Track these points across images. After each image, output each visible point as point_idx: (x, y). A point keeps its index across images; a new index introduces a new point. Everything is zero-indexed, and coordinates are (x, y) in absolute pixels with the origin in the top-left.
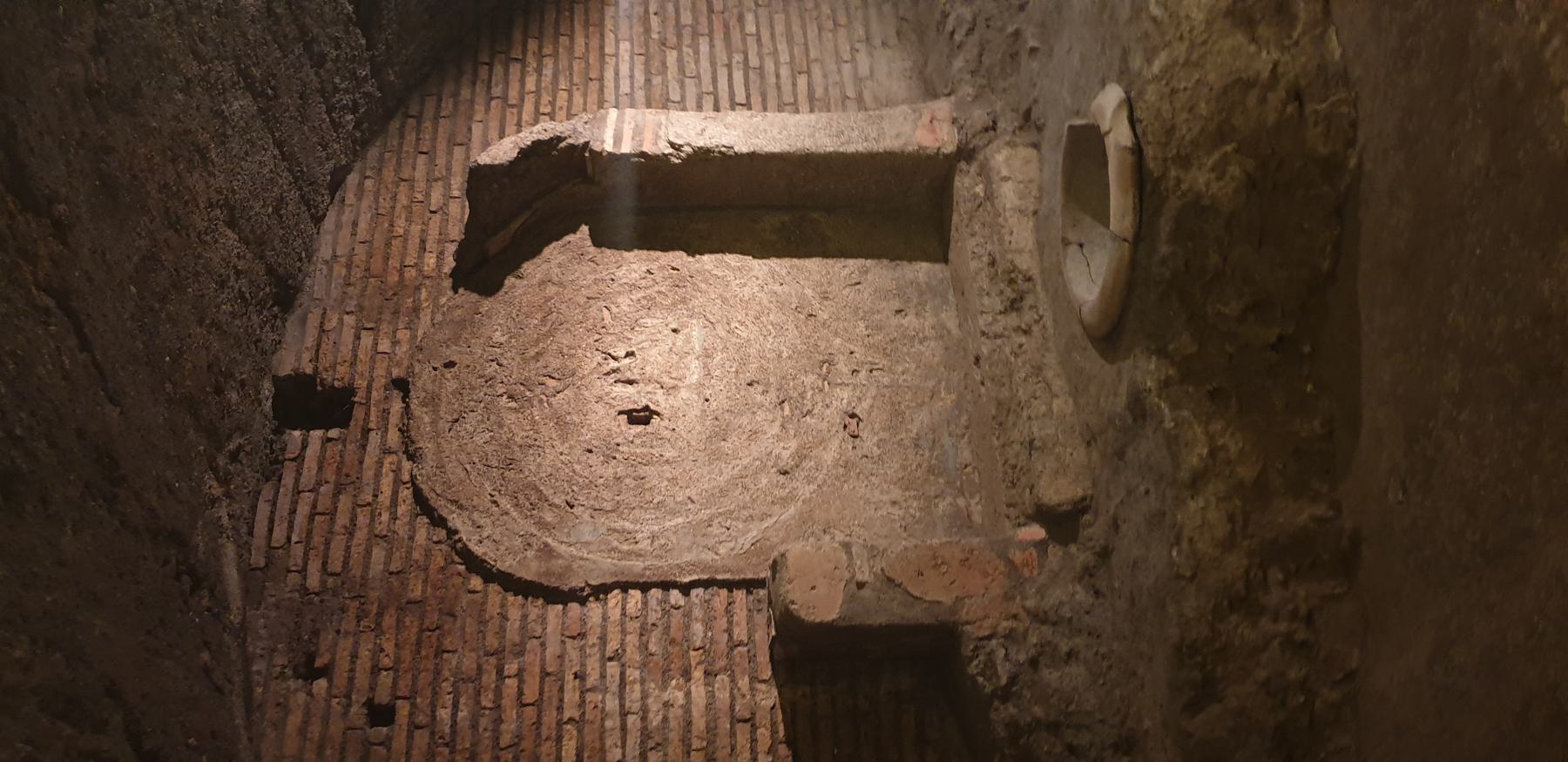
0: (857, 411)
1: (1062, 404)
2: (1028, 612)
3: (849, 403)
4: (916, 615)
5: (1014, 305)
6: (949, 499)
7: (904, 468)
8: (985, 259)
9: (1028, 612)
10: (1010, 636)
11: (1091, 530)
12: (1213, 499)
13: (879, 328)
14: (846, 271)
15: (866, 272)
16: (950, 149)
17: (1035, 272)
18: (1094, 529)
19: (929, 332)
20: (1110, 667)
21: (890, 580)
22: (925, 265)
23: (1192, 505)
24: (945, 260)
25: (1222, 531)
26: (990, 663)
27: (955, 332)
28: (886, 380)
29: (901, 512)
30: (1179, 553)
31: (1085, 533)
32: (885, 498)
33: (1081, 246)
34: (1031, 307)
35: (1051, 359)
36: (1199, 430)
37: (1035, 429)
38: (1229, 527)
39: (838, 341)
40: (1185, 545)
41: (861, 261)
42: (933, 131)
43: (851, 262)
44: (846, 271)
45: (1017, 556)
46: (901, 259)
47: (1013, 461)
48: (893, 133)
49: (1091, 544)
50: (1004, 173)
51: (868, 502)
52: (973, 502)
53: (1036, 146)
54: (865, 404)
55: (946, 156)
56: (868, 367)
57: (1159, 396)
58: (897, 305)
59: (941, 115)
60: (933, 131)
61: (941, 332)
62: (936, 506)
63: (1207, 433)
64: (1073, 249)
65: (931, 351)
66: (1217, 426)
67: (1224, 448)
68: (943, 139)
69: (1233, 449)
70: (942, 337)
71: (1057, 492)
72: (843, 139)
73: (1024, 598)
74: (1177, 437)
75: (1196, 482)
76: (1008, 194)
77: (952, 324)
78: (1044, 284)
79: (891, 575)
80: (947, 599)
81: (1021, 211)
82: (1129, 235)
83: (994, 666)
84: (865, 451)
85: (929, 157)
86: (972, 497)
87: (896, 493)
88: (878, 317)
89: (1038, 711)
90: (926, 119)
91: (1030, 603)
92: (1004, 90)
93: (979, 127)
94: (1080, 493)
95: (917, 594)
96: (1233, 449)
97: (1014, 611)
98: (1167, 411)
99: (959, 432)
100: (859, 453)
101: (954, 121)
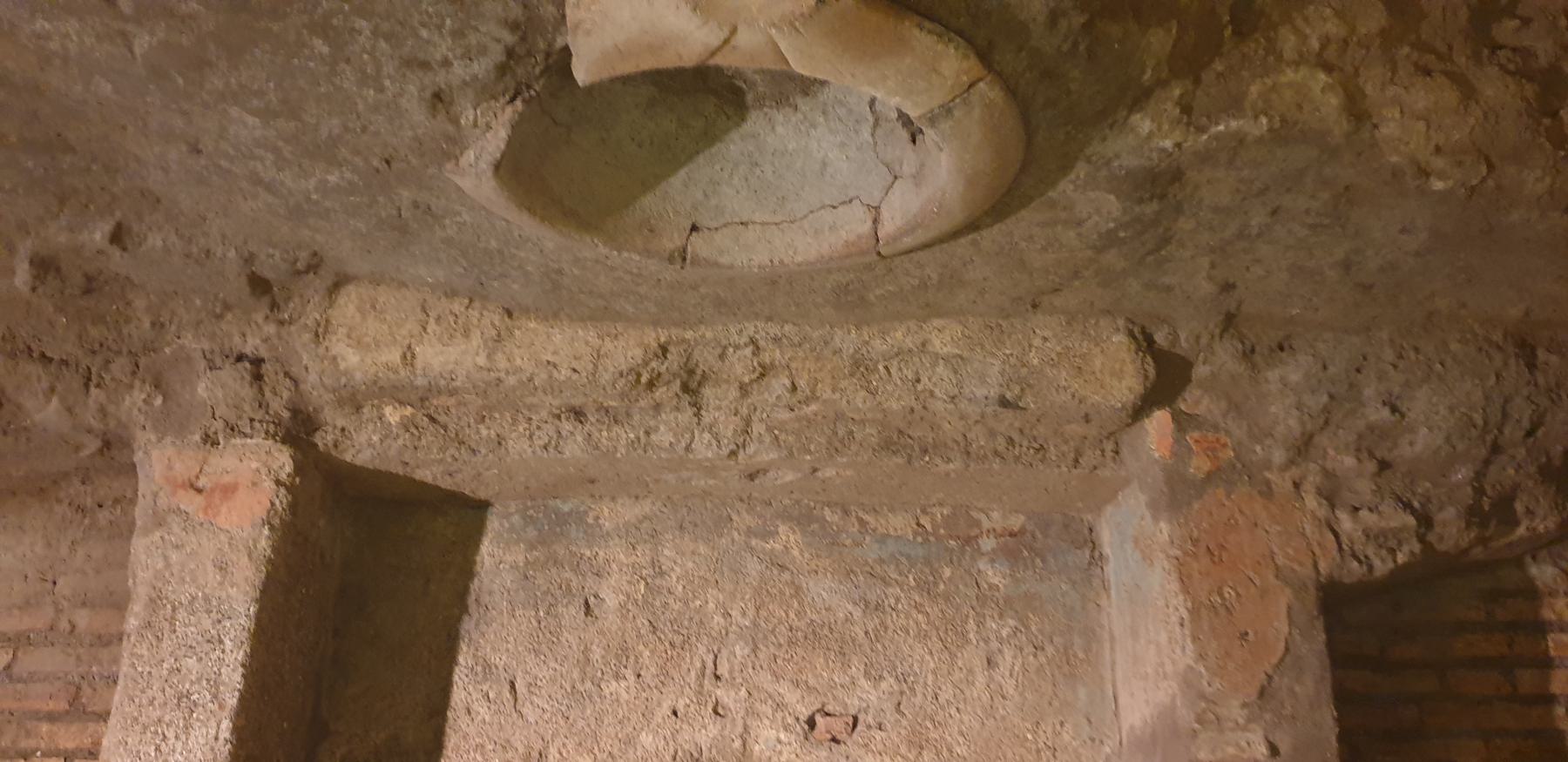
0: (804, 713)
1: (943, 338)
2: (1291, 462)
3: (786, 728)
4: (1313, 648)
5: (691, 386)
6: (982, 565)
7: (923, 636)
8: (567, 426)
9: (1291, 462)
10: (1330, 497)
11: (1183, 337)
12: (1391, 91)
13: (624, 651)
14: (482, 710)
15: (488, 667)
16: (283, 460)
17: (652, 337)
18: (1181, 335)
19: (643, 555)
20: (1417, 350)
21: (1262, 693)
22: (486, 547)
23: (1389, 130)
24: (483, 506)
25: (1451, 96)
26: (1376, 537)
27: (646, 507)
28: (741, 650)
29: (1008, 653)
30: (1442, 176)
31: (1184, 345)
32: (981, 680)
33: (694, 228)
34: (722, 357)
35: (847, 340)
36: (1290, 75)
37: (980, 392)
38: (1440, 79)
39: (646, 739)
40: (1439, 163)
41: (460, 676)
42: (229, 491)
43: (458, 696)
44: (482, 710)
45: (1199, 466)
46: (463, 594)
47: (1001, 444)
48: (213, 577)
49: (1204, 341)
50: (393, 356)
51: (990, 711)
52: (986, 524)
53: (339, 284)
54: (791, 696)
55: (299, 469)
56: (708, 683)
57: (1201, 130)
58: (571, 612)
59: (184, 466)
60: (229, 491)
61: (632, 534)
62: (991, 586)
63: (1297, 64)
64: (698, 245)
65: (681, 559)
66: (1288, 43)
67: (1326, 41)
68: (255, 474)
69: (1333, 28)
70: (654, 534)
71: (1119, 375)
72: (202, 695)
73: (1268, 465)
74: (1283, 120)
75: (1357, 111)
76: (442, 356)
77: (630, 511)
78: (683, 324)
79: (1253, 691)
80: (1283, 598)
81: (499, 339)
82: (973, 65)
83: (1383, 533)
84: (889, 706)
85: (293, 507)
86: (978, 524)
87: (972, 656)
88: (597, 654)
89: (1462, 474)
90: (190, 503)
91: (1279, 456)
92: (158, 325)
93: (247, 392)
94: (1120, 338)
95: (1282, 645)
96: (1333, 28)
97: (1289, 485)
98: (1234, 124)
99: (855, 529)
100: (890, 717)
101: (210, 440)
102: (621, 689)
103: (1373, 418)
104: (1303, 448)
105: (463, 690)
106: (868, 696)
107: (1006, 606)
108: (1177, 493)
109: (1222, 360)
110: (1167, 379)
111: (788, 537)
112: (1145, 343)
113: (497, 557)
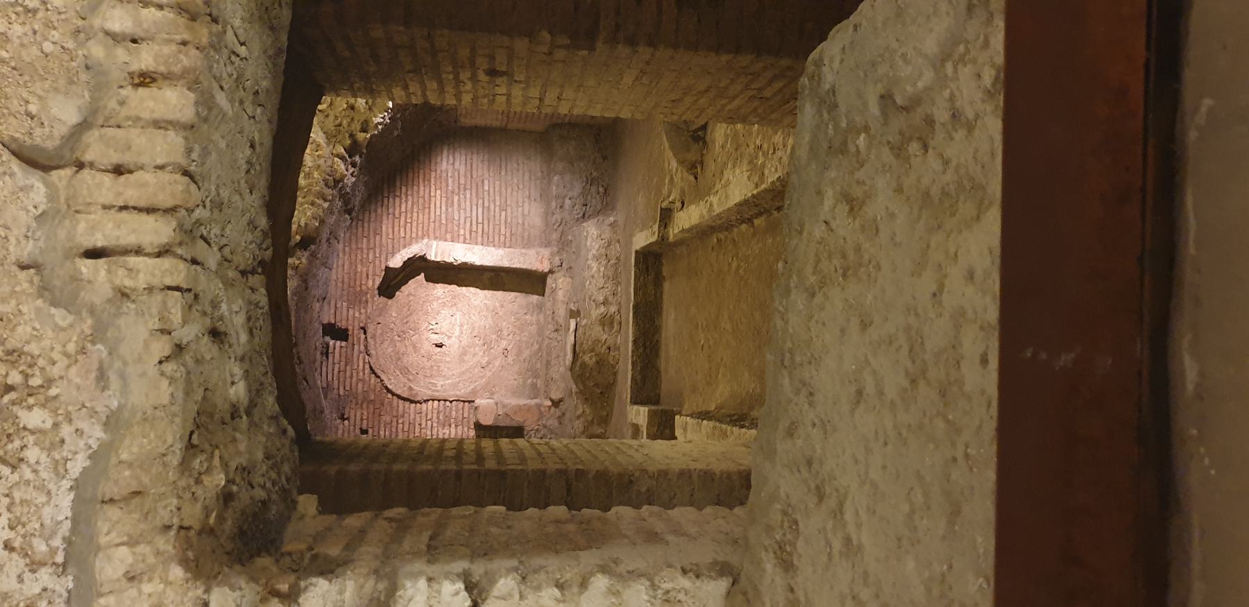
4: (514, 424)
16: (546, 270)
18: (563, 406)
61: (538, 321)
65: (533, 329)
68: (544, 267)
75: (579, 417)
76: (560, 293)
102: (513, 319)
103: (447, 102)
104: (545, 426)
105: (513, 294)
106: (510, 359)
107: (524, 383)
108: (539, 406)
109: (559, 413)
110: (556, 404)
111: (536, 347)
112: (561, 400)
113: (535, 298)
